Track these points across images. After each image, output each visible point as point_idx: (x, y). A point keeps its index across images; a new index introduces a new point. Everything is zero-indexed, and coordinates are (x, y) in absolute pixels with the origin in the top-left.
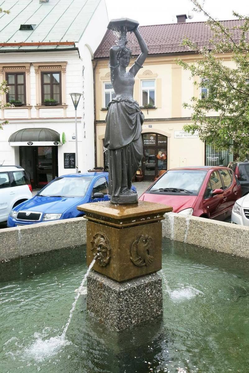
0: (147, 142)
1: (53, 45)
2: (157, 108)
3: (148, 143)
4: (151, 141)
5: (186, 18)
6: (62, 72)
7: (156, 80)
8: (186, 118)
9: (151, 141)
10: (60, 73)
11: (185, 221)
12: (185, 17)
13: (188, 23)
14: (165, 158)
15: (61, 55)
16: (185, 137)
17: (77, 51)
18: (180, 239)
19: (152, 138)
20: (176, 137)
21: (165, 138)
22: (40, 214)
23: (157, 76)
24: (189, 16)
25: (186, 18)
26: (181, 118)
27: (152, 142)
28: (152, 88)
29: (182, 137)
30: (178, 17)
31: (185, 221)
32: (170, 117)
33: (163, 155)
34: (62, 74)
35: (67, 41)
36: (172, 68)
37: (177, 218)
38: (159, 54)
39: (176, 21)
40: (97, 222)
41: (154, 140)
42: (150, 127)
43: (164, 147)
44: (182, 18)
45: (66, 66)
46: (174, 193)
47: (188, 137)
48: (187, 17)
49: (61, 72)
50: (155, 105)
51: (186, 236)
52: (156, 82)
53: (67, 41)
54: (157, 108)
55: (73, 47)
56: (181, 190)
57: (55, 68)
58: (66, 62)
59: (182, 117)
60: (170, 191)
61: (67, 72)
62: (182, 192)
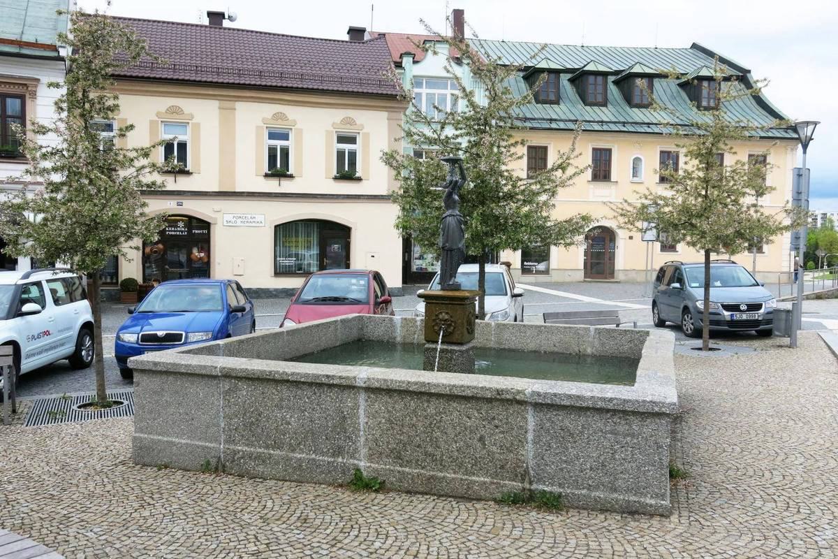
0: (172, 231)
1: (9, 43)
2: (192, 173)
3: (173, 233)
4: (179, 229)
5: (224, 18)
6: (27, 96)
7: (190, 124)
8: (243, 193)
9: (179, 229)
10: (22, 98)
11: (416, 321)
12: (222, 15)
13: (225, 29)
14: (206, 260)
15: (26, 66)
16: (242, 224)
17: (63, 63)
18: (408, 341)
19: (181, 224)
20: (225, 224)
21: (206, 225)
22: (182, 335)
23: (193, 118)
24: (229, 17)
25: (224, 18)
26: (235, 192)
27: (182, 232)
28: (181, 138)
29: (237, 224)
30: (210, 14)
31: (416, 321)
32: (217, 190)
33: (202, 255)
34: (28, 102)
35: (36, 41)
36: (220, 108)
37: (405, 319)
38: (192, 81)
39: (206, 21)
40: (438, 303)
41: (184, 227)
42: (180, 204)
43: (205, 242)
44: (216, 17)
45: (36, 86)
46: (336, 302)
47: (248, 224)
48: (227, 17)
49: (25, 96)
50: (189, 167)
51: (416, 336)
52: (189, 129)
53: (36, 41)
54: (192, 173)
55: (53, 54)
56: (345, 299)
57: (12, 87)
58: (38, 80)
59: (237, 191)
60: (330, 300)
61: (38, 98)
62: (346, 301)
